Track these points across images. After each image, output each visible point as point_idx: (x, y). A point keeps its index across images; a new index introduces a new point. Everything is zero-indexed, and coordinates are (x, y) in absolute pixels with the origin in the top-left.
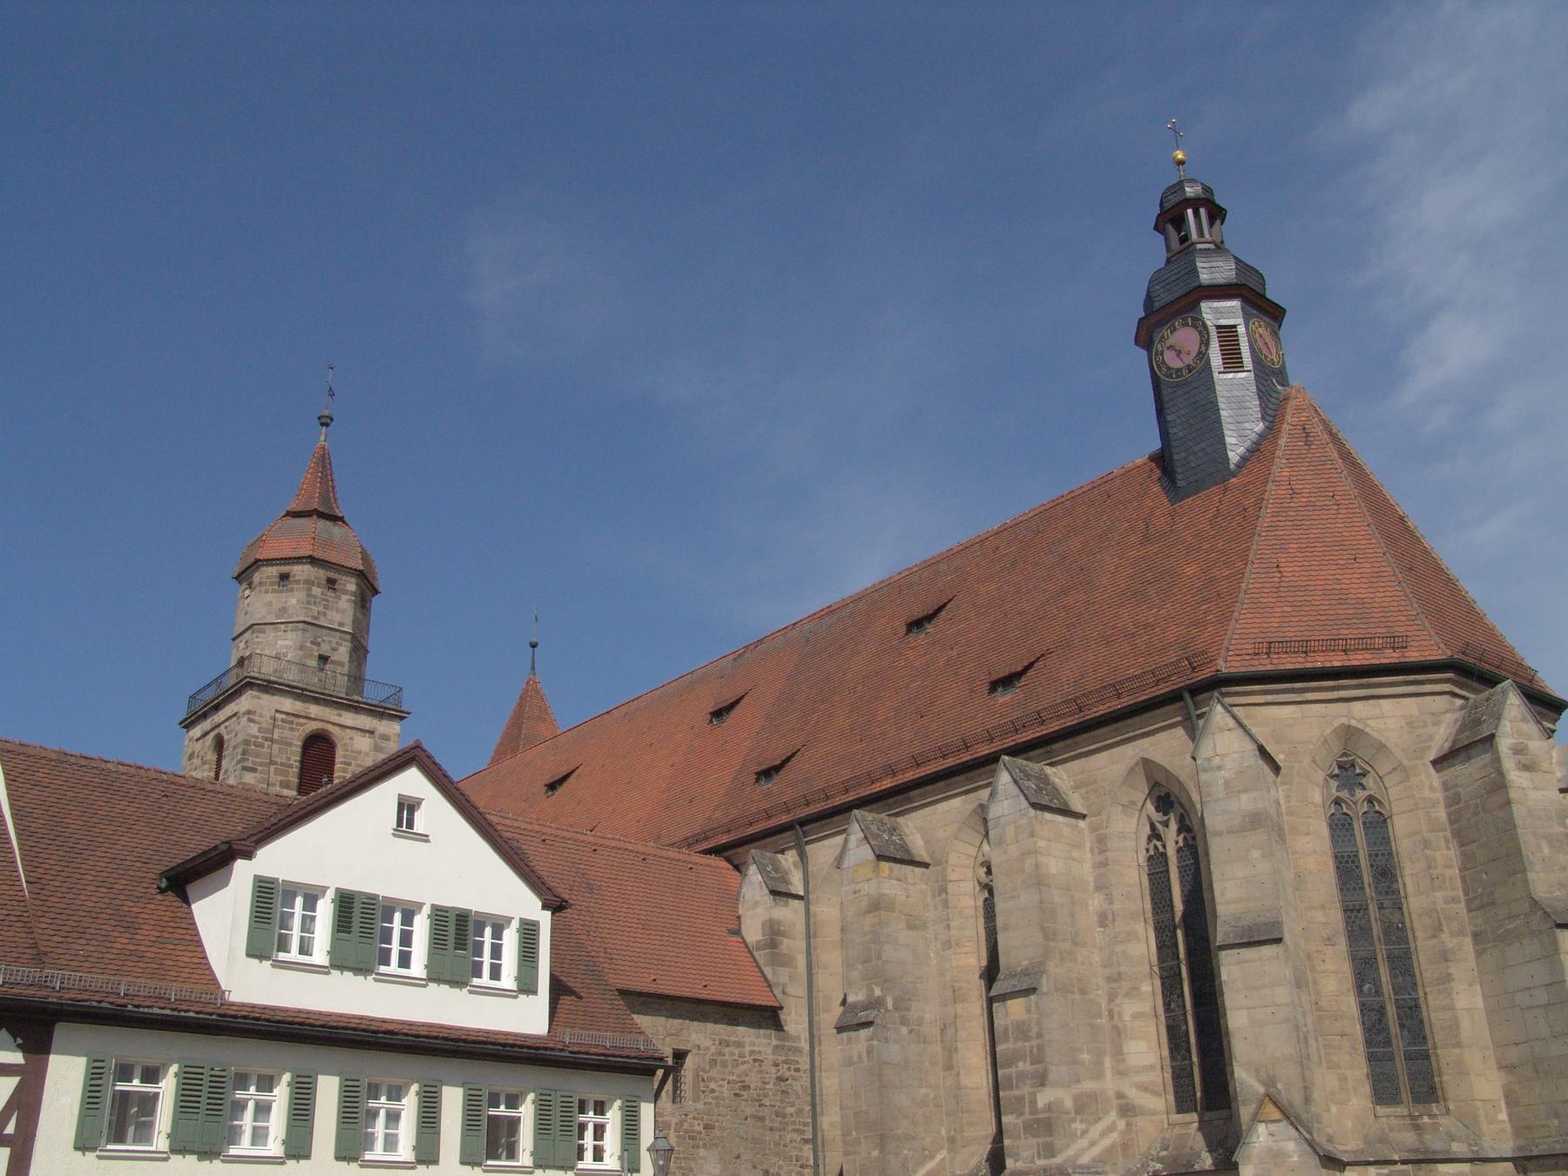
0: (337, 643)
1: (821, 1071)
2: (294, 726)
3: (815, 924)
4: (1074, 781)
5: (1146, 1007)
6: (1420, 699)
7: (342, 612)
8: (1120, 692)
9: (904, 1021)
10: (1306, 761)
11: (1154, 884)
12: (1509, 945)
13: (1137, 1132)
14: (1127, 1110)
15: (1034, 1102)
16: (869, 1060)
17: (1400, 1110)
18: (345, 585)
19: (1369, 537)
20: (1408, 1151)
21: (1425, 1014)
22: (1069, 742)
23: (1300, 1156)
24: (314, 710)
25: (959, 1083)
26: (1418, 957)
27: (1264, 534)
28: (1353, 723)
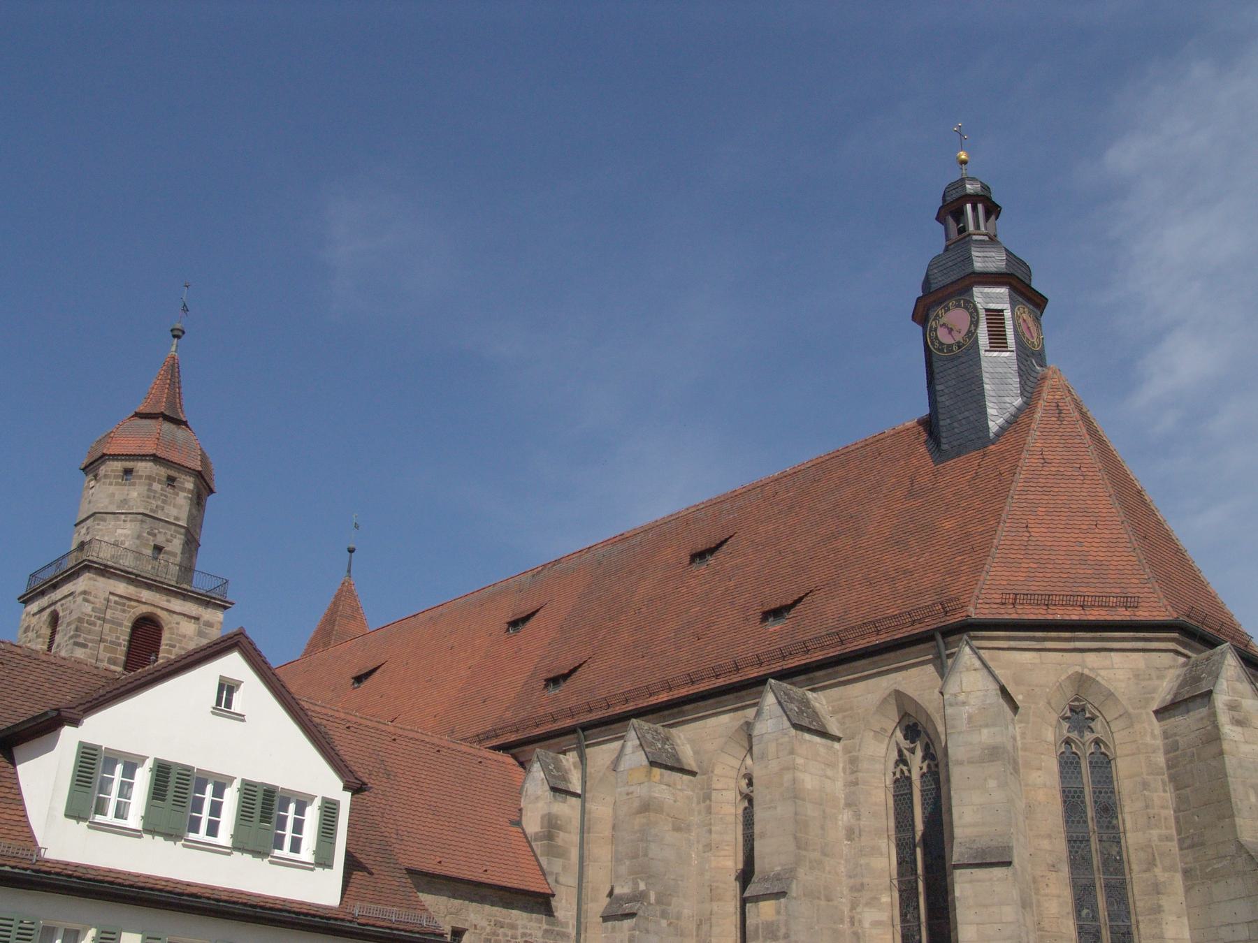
0: (172, 535)
2: (126, 608)
3: (589, 820)
4: (833, 707)
5: (884, 916)
7: (179, 507)
9: (664, 914)
18: (183, 484)
22: (830, 670)
24: (146, 595)
28: (1086, 672)
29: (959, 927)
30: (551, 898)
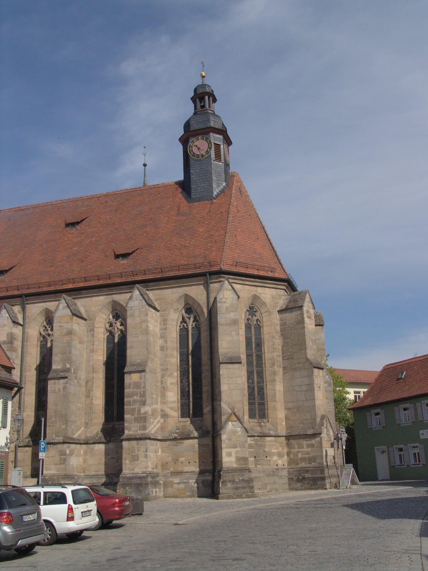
1: (24, 394)
3: (27, 336)
5: (175, 381)
6: (276, 290)
8: (180, 268)
10: (243, 304)
11: (181, 338)
12: (296, 371)
13: (168, 424)
14: (165, 416)
15: (139, 411)
16: (63, 391)
17: (255, 420)
19: (261, 232)
20: (259, 433)
21: (265, 391)
22: (157, 283)
23: (242, 433)
25: (92, 403)
26: (266, 373)
27: (230, 223)
28: (257, 294)
29: (221, 385)
30: (13, 370)
